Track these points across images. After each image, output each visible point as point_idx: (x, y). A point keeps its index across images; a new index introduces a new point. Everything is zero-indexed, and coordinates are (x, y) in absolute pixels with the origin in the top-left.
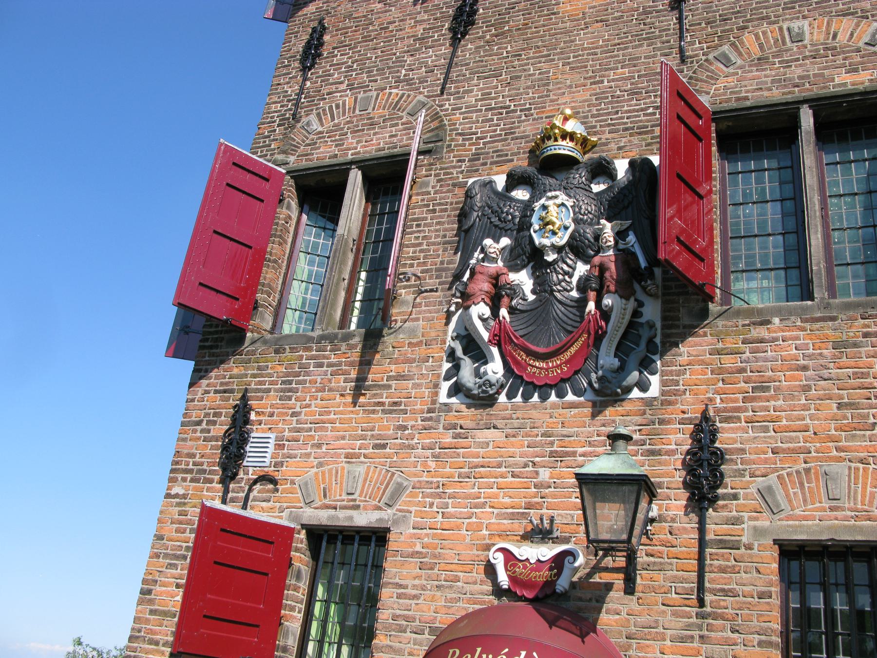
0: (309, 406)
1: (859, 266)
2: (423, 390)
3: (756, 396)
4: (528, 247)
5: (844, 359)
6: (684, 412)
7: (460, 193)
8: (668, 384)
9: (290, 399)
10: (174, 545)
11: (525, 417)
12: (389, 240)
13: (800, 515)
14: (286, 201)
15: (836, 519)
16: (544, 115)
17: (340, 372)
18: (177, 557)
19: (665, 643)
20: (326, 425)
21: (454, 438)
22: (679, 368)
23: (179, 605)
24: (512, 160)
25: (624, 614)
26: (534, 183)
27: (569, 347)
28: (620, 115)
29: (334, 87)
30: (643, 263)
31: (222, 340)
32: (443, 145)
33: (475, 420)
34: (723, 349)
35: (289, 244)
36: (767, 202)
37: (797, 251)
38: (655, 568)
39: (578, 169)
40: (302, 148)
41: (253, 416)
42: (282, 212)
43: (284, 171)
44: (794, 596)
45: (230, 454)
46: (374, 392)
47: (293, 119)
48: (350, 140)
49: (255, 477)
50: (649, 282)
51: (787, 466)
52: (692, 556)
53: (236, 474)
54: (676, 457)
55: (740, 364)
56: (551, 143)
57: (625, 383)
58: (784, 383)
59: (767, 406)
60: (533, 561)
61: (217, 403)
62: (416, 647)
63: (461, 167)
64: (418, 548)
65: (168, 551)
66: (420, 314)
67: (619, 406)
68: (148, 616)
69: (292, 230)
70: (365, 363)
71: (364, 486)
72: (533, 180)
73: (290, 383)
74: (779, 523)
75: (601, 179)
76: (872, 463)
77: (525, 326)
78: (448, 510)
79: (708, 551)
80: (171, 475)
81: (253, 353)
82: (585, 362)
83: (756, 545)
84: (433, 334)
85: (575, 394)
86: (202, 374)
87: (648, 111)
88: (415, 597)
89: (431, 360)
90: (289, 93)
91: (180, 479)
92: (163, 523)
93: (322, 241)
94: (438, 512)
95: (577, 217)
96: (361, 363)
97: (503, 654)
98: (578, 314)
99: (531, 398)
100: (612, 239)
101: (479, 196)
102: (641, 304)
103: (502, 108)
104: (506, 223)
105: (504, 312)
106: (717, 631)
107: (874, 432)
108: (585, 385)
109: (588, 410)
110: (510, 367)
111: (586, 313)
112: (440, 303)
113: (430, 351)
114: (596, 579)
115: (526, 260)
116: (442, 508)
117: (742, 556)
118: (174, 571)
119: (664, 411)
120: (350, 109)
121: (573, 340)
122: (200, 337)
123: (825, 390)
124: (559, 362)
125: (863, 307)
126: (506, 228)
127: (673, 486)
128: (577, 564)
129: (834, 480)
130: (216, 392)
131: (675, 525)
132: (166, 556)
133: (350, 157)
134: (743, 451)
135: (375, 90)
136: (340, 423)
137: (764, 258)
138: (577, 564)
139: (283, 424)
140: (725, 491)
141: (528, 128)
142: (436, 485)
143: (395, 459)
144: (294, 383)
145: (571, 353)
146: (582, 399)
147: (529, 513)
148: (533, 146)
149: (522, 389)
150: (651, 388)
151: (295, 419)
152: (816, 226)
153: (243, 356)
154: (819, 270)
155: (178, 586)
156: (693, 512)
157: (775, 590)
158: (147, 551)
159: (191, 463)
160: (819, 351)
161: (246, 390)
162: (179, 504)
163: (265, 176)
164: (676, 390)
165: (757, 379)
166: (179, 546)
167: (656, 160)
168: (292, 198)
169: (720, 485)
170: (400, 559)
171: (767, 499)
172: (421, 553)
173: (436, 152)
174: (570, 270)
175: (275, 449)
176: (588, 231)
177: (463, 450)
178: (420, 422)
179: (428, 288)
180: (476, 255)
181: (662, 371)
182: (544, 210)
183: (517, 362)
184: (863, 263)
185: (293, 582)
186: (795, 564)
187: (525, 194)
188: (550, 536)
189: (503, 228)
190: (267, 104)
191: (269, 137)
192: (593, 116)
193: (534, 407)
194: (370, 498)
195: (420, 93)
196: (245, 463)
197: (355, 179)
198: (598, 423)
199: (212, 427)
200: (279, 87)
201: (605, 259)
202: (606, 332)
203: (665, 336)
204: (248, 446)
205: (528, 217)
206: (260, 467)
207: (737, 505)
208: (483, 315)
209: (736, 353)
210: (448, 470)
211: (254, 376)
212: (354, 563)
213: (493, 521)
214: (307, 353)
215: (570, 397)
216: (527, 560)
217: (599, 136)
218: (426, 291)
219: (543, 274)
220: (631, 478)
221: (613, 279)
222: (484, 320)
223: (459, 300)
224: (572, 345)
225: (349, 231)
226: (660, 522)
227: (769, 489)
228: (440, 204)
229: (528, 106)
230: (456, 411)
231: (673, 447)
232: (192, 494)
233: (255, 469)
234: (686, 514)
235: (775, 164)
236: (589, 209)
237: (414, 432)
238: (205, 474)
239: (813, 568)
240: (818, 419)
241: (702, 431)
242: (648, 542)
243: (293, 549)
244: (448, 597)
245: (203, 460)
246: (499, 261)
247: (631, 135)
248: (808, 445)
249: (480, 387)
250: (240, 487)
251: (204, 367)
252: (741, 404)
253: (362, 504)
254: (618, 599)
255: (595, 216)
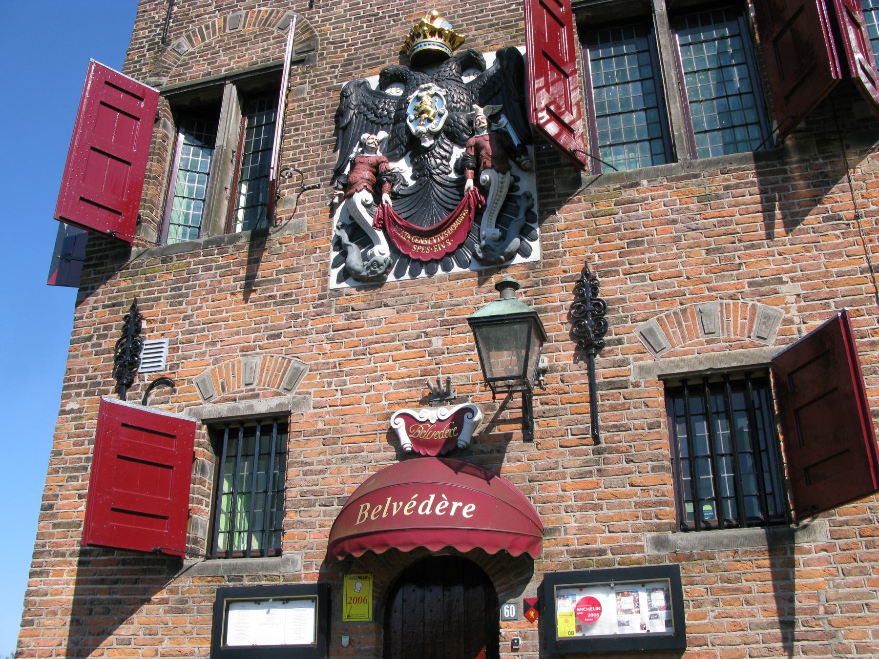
0: (200, 308)
1: (716, 133)
2: (313, 279)
3: (631, 251)
4: (405, 136)
5: (709, 210)
6: (565, 272)
7: (336, 96)
8: (549, 248)
9: (181, 304)
10: (73, 459)
11: (415, 292)
12: (268, 149)
13: (681, 351)
14: (162, 121)
15: (713, 351)
16: (412, 19)
17: (229, 273)
18: (77, 469)
19: (566, 481)
20: (219, 324)
21: (346, 320)
22: (557, 232)
23: (83, 514)
24: (384, 62)
25: (525, 460)
26: (407, 79)
27: (452, 223)
28: (485, 13)
29: (202, 10)
30: (516, 141)
31: (107, 257)
32: (315, 56)
33: (366, 301)
34: (597, 212)
35: (168, 162)
36: (628, 82)
37: (659, 124)
38: (551, 414)
39: (448, 63)
40: (174, 69)
41: (144, 325)
42: (159, 131)
43: (158, 91)
44: (680, 428)
45: (124, 362)
46: (264, 287)
47: (163, 43)
48: (223, 58)
49: (151, 382)
50: (523, 157)
51: (665, 309)
52: (584, 399)
53: (132, 381)
54: (562, 312)
55: (614, 224)
56: (421, 40)
57: (507, 250)
58: (656, 236)
59: (642, 259)
60: (433, 421)
61: (107, 317)
62: (326, 518)
63: (334, 72)
64: (320, 426)
65: (68, 465)
66: (304, 210)
67: (503, 273)
68: (51, 530)
69: (170, 148)
70: (254, 261)
71: (261, 375)
72: (406, 76)
73: (180, 289)
74: (661, 360)
75: (471, 71)
76: (740, 298)
77: (407, 209)
78: (347, 387)
79: (599, 393)
80: (65, 392)
81: (140, 265)
82: (468, 236)
83: (643, 382)
84: (319, 227)
85: (460, 266)
86: (89, 291)
87: (512, 8)
88: (322, 472)
89: (318, 251)
90: (156, 18)
91: (73, 395)
92: (59, 439)
93: (200, 159)
94: (337, 390)
95: (451, 106)
96: (249, 262)
97: (414, 499)
98: (457, 193)
99: (419, 274)
100: (485, 121)
101: (354, 95)
102: (517, 179)
103: (370, 16)
104: (382, 118)
105: (386, 197)
106: (614, 464)
107: (740, 271)
108: (470, 257)
109: (474, 280)
110: (396, 247)
111: (465, 190)
112: (324, 198)
113: (317, 242)
114: (496, 431)
115: (404, 149)
116: (341, 386)
117: (631, 393)
118: (75, 483)
119: (546, 273)
120: (219, 29)
121: (455, 216)
122: (82, 264)
123: (694, 239)
124: (443, 238)
125: (723, 164)
126: (383, 123)
127: (561, 338)
128: (476, 419)
129: (708, 316)
130: (104, 307)
131: (566, 373)
132: (65, 470)
133: (223, 72)
134: (623, 300)
135: (244, 9)
136: (233, 320)
137: (630, 132)
138: (476, 419)
139: (175, 328)
140: (609, 338)
141: (398, 32)
142: (333, 365)
143: (290, 346)
144: (184, 289)
145: (453, 228)
146: (468, 270)
147: (426, 379)
148: (403, 47)
149: (409, 267)
150: (533, 253)
151: (187, 322)
152: (675, 97)
153: (130, 270)
154: (681, 134)
155: (80, 497)
156: (581, 360)
157: (663, 420)
158: (45, 468)
159: (84, 378)
160: (685, 206)
161: (136, 301)
162: (74, 419)
163: (139, 95)
164: (557, 252)
165: (631, 235)
166: (78, 458)
167: (522, 50)
168: (167, 118)
169: (605, 332)
170: (303, 438)
171: (649, 340)
172: (323, 430)
173: (309, 61)
174: (447, 155)
175: (170, 353)
176: (461, 117)
177: (356, 330)
178: (312, 309)
179: (310, 185)
180: (355, 150)
181: (542, 237)
182: (418, 101)
183: (402, 243)
184: (719, 130)
185: (198, 476)
186: (679, 402)
187: (398, 91)
188: (448, 398)
189: (379, 123)
190: (135, 31)
191: (139, 62)
192: (459, 16)
193: (422, 282)
194: (268, 386)
195: (289, 8)
196: (140, 370)
197: (230, 93)
198: (486, 290)
199: (103, 341)
200: (146, 13)
201: (481, 139)
202: (485, 206)
203: (541, 205)
204: (142, 354)
205: (403, 109)
206: (155, 372)
207: (622, 349)
208: (366, 201)
209: (610, 215)
210: (343, 350)
211: (143, 287)
212: (257, 455)
213: (392, 391)
214: (194, 259)
215: (456, 269)
216: (428, 421)
217: (467, 34)
218: (309, 188)
219: (421, 159)
220: (521, 316)
221: (489, 156)
222: (367, 206)
223: (342, 192)
224: (454, 221)
225: (227, 142)
226: (552, 372)
227: (651, 331)
228: (316, 108)
229: (396, 12)
230: (347, 295)
231: (558, 303)
232: (87, 407)
233: (150, 374)
234: (575, 362)
235: (633, 49)
236: (462, 98)
237: (307, 319)
238: (99, 386)
239: (696, 404)
240: (690, 265)
241: (584, 286)
242: (542, 392)
243: (195, 444)
244: (354, 468)
245: (96, 373)
246: (378, 151)
247: (496, 30)
248: (682, 288)
249: (368, 268)
250: (137, 393)
251: (90, 285)
252: (619, 259)
253: (261, 392)
254: (518, 447)
255: (468, 104)
